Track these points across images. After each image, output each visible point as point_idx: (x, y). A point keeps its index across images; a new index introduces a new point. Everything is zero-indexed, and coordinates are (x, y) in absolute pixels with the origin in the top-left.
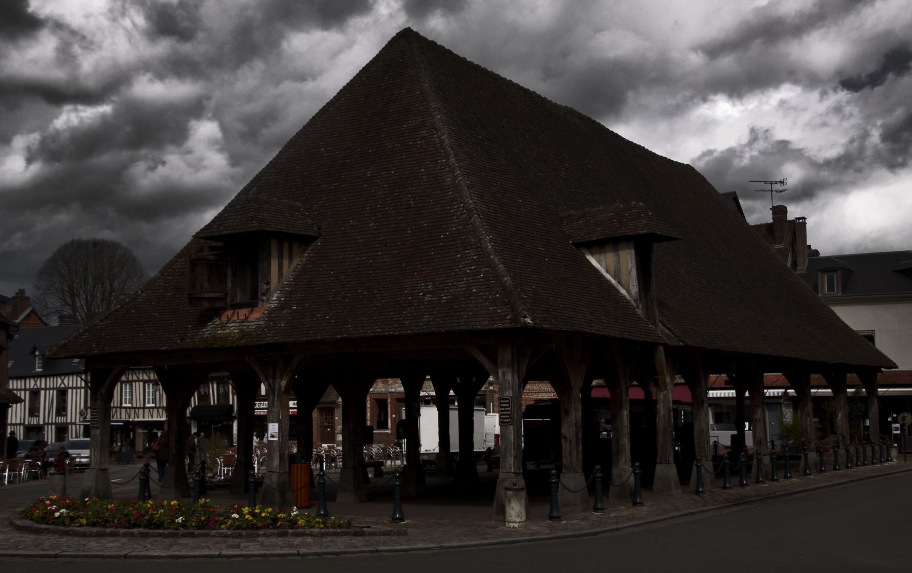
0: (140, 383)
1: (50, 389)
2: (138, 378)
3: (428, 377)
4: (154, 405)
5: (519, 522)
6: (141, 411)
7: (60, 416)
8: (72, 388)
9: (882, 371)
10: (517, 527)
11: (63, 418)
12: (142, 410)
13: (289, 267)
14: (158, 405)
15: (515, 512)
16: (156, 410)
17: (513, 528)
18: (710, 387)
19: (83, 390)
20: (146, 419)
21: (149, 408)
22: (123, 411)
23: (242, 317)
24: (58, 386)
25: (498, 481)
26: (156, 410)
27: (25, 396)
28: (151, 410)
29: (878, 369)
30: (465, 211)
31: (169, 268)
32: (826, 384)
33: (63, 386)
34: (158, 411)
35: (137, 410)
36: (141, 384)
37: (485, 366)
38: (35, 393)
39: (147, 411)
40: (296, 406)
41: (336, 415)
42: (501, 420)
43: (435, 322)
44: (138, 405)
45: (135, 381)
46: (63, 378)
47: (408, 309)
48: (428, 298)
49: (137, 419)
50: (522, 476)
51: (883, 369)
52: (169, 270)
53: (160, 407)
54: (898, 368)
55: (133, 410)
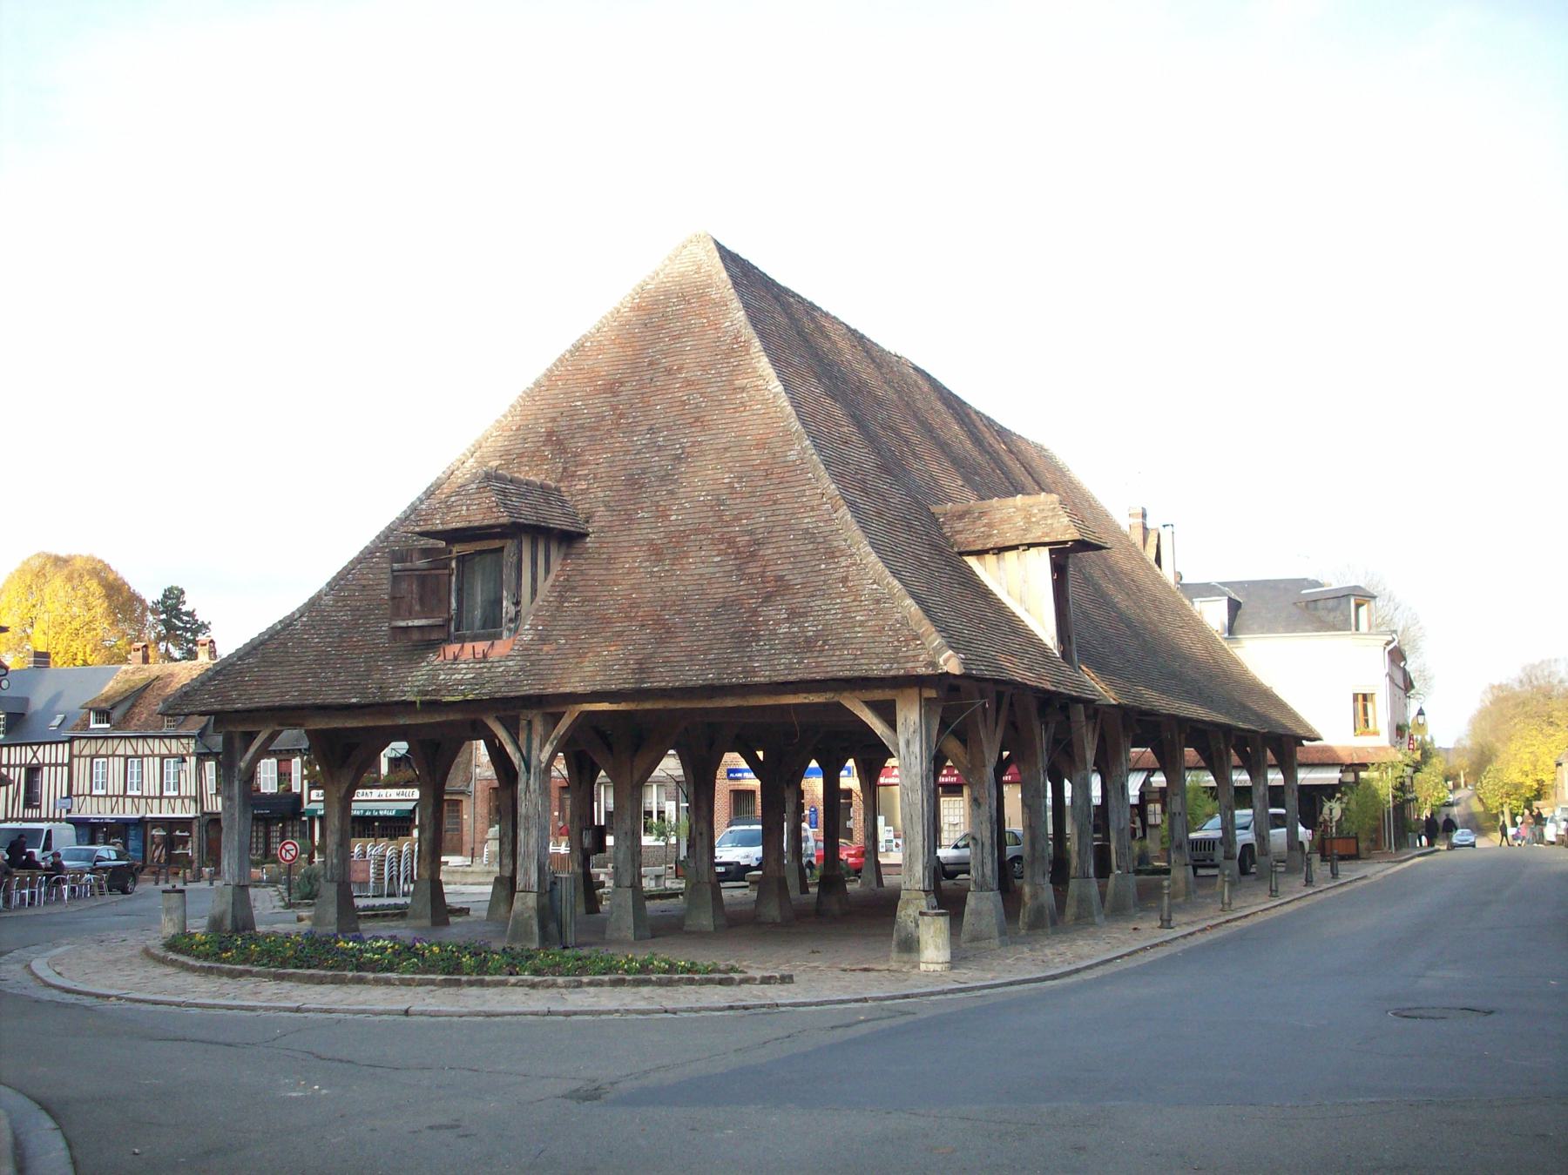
0: (156, 758)
1: (15, 766)
2: (153, 752)
3: (671, 752)
4: (176, 793)
5: (942, 963)
6: (156, 802)
7: (30, 807)
8: (50, 765)
9: (1303, 745)
10: (939, 970)
11: (34, 810)
12: (158, 801)
13: (546, 579)
14: (183, 794)
15: (934, 949)
16: (179, 801)
17: (934, 971)
18: (1132, 767)
19: (66, 769)
20: (163, 815)
21: (169, 798)
22: (128, 801)
23: (450, 656)
24: (28, 762)
25: (900, 903)
26: (179, 801)
27: (19, 775)
28: (172, 801)
29: (1298, 740)
30: (825, 500)
31: (342, 579)
32: (1241, 764)
33: (35, 761)
34: (183, 802)
35: (149, 801)
36: (157, 760)
37: (876, 731)
38: (33, 771)
39: (165, 802)
40: (322, 798)
41: (464, 812)
42: (356, 834)
43: (803, 665)
44: (152, 794)
45: (148, 756)
46: (35, 748)
47: (754, 644)
48: (783, 629)
49: (149, 815)
50: (933, 895)
51: (1305, 742)
52: (342, 582)
53: (186, 797)
54: (1320, 739)
55: (144, 800)
